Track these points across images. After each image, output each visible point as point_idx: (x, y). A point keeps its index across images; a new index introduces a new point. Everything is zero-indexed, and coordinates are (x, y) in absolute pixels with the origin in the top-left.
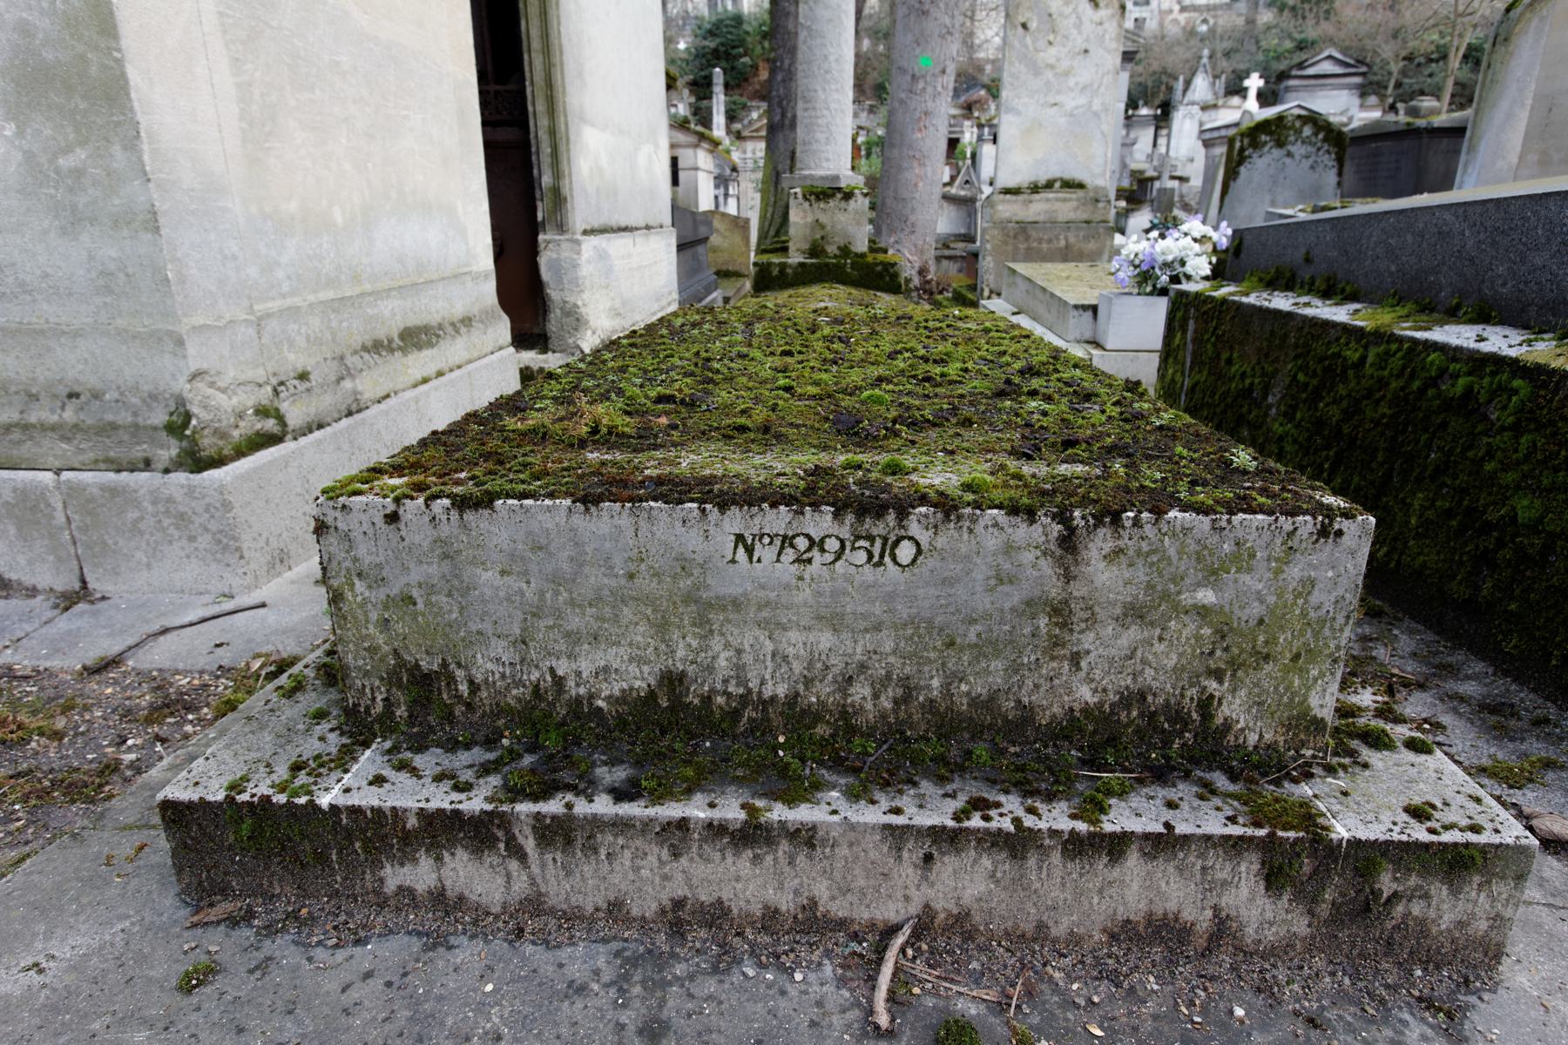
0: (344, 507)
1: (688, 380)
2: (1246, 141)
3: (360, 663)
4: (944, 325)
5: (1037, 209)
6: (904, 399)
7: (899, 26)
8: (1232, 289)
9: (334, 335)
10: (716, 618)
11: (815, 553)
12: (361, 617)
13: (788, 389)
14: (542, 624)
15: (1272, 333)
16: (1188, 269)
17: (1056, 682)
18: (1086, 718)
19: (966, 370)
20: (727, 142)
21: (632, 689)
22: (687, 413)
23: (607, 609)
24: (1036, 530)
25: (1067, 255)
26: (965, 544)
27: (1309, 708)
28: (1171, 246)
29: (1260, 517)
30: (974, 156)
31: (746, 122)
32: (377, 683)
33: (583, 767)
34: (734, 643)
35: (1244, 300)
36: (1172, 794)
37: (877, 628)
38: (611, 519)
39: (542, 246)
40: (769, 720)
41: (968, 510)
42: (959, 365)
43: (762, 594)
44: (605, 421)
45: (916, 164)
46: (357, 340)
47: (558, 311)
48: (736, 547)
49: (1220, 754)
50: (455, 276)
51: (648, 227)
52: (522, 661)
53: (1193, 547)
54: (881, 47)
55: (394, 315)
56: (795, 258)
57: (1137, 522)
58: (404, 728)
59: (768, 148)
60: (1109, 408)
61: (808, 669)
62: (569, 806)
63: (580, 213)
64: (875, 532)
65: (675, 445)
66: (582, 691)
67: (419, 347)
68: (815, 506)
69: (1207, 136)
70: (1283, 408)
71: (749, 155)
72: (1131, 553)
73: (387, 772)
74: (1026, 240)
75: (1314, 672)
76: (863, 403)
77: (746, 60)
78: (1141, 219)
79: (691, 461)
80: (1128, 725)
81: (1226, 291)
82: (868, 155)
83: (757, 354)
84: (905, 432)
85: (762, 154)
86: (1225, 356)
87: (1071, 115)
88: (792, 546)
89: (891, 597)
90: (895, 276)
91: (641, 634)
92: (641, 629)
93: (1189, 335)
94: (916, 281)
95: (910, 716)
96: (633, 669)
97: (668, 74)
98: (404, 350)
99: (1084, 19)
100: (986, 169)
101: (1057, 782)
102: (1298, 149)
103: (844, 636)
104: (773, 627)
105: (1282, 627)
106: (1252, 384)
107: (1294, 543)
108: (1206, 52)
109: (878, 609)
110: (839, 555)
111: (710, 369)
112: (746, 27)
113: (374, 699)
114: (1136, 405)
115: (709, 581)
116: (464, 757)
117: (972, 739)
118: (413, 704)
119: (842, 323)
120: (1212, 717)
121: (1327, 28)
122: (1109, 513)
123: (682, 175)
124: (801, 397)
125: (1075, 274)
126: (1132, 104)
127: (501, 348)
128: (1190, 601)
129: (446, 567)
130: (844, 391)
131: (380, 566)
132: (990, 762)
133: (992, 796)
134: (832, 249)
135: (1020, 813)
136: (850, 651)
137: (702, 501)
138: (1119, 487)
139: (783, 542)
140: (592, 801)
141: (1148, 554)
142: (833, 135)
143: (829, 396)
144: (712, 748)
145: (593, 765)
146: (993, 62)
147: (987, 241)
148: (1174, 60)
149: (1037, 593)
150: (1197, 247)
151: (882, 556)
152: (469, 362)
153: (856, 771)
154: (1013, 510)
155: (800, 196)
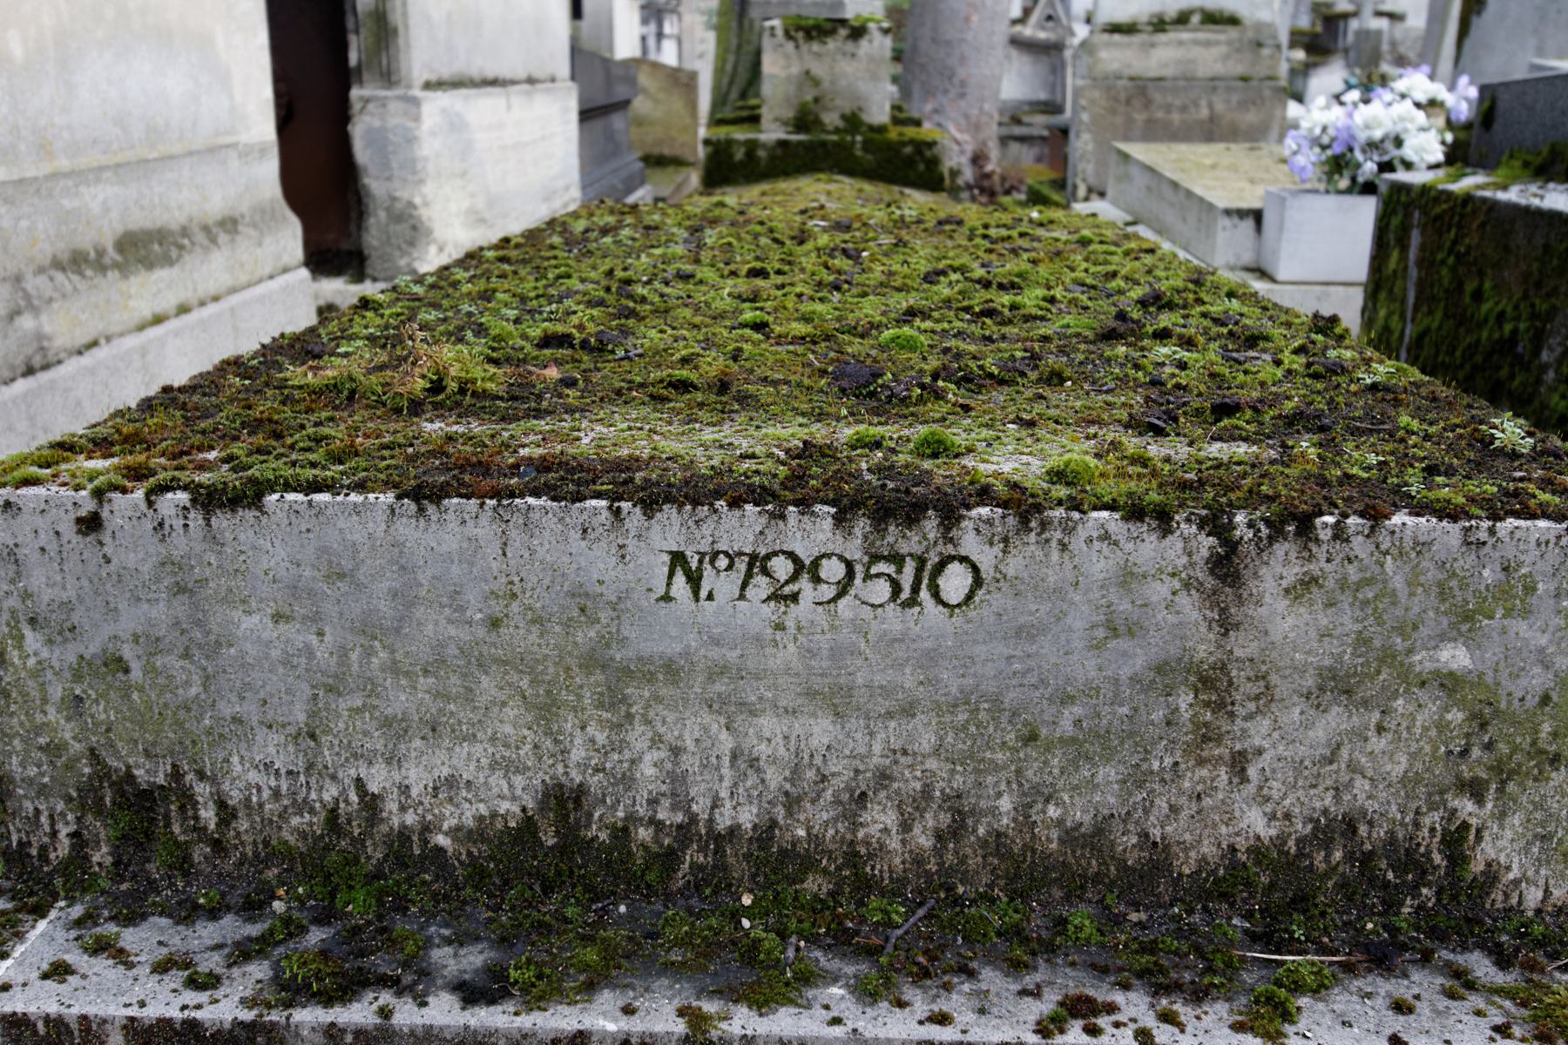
0: (8, 504)
1: (595, 312)
3: (32, 771)
4: (1014, 233)
6: (952, 343)
10: (638, 693)
11: (804, 584)
12: (35, 694)
13: (759, 327)
14: (343, 705)
15: (1547, 248)
16: (1408, 152)
17: (1207, 802)
18: (1258, 863)
19: (1052, 300)
21: (494, 815)
22: (590, 359)
23: (454, 679)
24: (1174, 544)
25: (1211, 131)
26: (1055, 569)
32: (60, 806)
33: (410, 947)
34: (669, 737)
35: (1501, 196)
36: (1401, 989)
37: (908, 711)
38: (462, 526)
39: (356, 106)
40: (725, 868)
41: (1059, 513)
42: (1040, 292)
44: (453, 372)
46: (44, 251)
47: (382, 215)
48: (671, 575)
49: (1481, 923)
50: (212, 150)
51: (531, 81)
52: (310, 767)
53: (1433, 575)
55: (106, 210)
56: (771, 133)
57: (1339, 533)
58: (104, 883)
60: (1287, 357)
61: (792, 781)
62: (385, 1013)
63: (421, 54)
64: (904, 548)
65: (570, 410)
66: (410, 818)
67: (150, 264)
68: (804, 504)
72: (1330, 584)
73: (74, 957)
74: (1144, 106)
76: (883, 348)
78: (1330, 77)
79: (596, 435)
80: (1326, 876)
81: (1470, 182)
83: (705, 272)
84: (953, 393)
86: (1470, 287)
88: (766, 572)
89: (931, 658)
90: (934, 162)
91: (511, 722)
92: (510, 712)
93: (1413, 253)
94: (968, 174)
95: (963, 861)
96: (498, 782)
98: (123, 269)
101: (1210, 970)
103: (852, 724)
104: (733, 710)
106: (1515, 331)
109: (908, 678)
110: (843, 588)
111: (630, 297)
114: (1332, 354)
116: (208, 931)
117: (1067, 898)
118: (122, 841)
119: (848, 228)
120: (1466, 860)
122: (1294, 516)
124: (780, 339)
127: (286, 270)
128: (1429, 666)
129: (181, 607)
130: (852, 330)
131: (67, 606)
132: (1097, 938)
133: (1102, 993)
134: (831, 119)
135: (1149, 1021)
136: (862, 750)
137: (614, 497)
139: (751, 566)
140: (424, 1004)
141: (1359, 586)
143: (828, 338)
144: (631, 917)
145: (428, 943)
147: (1080, 109)
149: (1174, 650)
150: (1420, 116)
151: (916, 589)
152: (233, 290)
153: (871, 952)
154: (1134, 512)
155: (780, 32)
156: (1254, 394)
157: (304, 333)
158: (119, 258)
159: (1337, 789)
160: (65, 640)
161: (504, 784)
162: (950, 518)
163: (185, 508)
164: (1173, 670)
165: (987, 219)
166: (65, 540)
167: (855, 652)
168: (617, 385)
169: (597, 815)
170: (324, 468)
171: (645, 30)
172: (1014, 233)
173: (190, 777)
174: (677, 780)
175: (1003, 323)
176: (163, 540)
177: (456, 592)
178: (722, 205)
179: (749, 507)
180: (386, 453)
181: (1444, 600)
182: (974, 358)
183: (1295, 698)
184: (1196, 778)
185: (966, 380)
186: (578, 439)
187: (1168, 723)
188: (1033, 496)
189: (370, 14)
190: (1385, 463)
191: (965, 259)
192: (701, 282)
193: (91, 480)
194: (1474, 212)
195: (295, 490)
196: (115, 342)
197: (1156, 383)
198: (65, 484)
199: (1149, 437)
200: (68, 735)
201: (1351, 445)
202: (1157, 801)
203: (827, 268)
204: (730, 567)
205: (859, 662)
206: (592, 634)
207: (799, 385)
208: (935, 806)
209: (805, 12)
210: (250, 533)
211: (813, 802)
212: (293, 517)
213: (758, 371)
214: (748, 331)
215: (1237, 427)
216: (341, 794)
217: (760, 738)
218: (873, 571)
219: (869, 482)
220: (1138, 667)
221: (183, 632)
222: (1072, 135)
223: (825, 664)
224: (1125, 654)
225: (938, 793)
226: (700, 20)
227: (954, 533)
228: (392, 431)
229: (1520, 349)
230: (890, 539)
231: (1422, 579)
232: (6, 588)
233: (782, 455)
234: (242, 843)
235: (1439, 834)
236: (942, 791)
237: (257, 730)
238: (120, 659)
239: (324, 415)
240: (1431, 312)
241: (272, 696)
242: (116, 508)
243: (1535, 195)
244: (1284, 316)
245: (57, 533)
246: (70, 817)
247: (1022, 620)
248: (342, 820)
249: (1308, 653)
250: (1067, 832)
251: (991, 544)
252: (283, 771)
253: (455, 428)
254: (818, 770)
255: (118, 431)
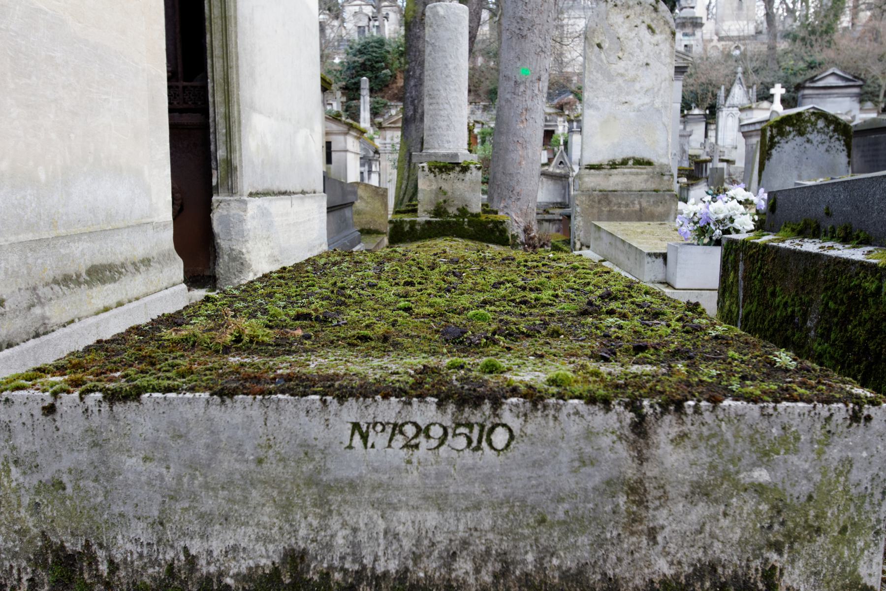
0: (7, 400)
1: (324, 303)
2: (775, 131)
3: (10, 544)
4: (540, 264)
5: (616, 180)
6: (504, 317)
7: (504, 46)
8: (771, 237)
9: (29, 271)
10: (335, 499)
11: (422, 439)
12: (14, 502)
13: (407, 309)
14: (179, 506)
15: (805, 270)
16: (736, 225)
17: (637, 555)
19: (557, 296)
20: (371, 131)
21: (257, 566)
24: (612, 417)
25: (641, 216)
26: (551, 430)
27: (859, 577)
28: (722, 207)
29: (801, 404)
30: (566, 143)
31: (386, 117)
32: (24, 564)
34: (351, 522)
35: (781, 245)
37: (477, 507)
38: (244, 410)
39: (215, 205)
41: (553, 401)
42: (551, 292)
43: (375, 476)
44: (247, 332)
45: (519, 148)
46: (49, 275)
47: (226, 257)
48: (353, 434)
50: (139, 225)
51: (303, 192)
52: (159, 541)
53: (746, 432)
54: (492, 63)
55: (83, 254)
56: (422, 217)
57: (697, 410)
59: (404, 136)
60: (673, 323)
61: (416, 546)
63: (247, 180)
64: (473, 419)
66: (212, 569)
67: (103, 282)
68: (421, 397)
69: (746, 129)
70: (819, 331)
71: (388, 141)
72: (694, 437)
75: (861, 544)
76: (469, 320)
77: (387, 71)
78: (699, 191)
79: (316, 364)
82: (483, 142)
83: (383, 284)
84: (503, 341)
85: (399, 140)
86: (769, 290)
87: (639, 110)
88: (402, 433)
89: (488, 478)
90: (504, 231)
91: (267, 515)
92: (267, 510)
94: (522, 237)
96: (260, 548)
97: (323, 80)
99: (644, 41)
100: (575, 153)
102: (815, 137)
103: (449, 514)
104: (385, 507)
105: (828, 503)
106: (793, 312)
107: (831, 427)
108: (740, 69)
109: (477, 489)
110: (442, 441)
111: (343, 295)
112: (387, 48)
113: (20, 579)
115: (328, 465)
119: (457, 262)
121: (830, 54)
122: (673, 402)
123: (334, 156)
125: (648, 230)
126: (686, 105)
127: (174, 285)
128: (748, 480)
129: (95, 454)
130: (454, 311)
131: (35, 454)
134: (452, 210)
136: (453, 528)
138: (680, 382)
139: (394, 430)
142: (453, 120)
143: (441, 315)
146: (579, 74)
148: (719, 74)
149: (615, 473)
151: (480, 441)
152: (147, 295)
154: (591, 400)
155: (426, 169)
156: (656, 341)
157: (174, 314)
158: (88, 279)
159: (705, 548)
160: (33, 472)
161: (263, 549)
162: (497, 404)
163: (100, 401)
164: (615, 484)
165: (526, 258)
166: (35, 418)
167: (449, 475)
168: (332, 338)
169: (312, 566)
170: (174, 380)
171: (362, 169)
172: (540, 264)
173: (95, 547)
174: (355, 546)
175: (531, 307)
176: (87, 418)
177: (240, 445)
178: (396, 252)
179: (393, 399)
180: (208, 372)
181: (753, 445)
182: (515, 324)
183: (680, 498)
184: (630, 542)
185: (509, 335)
186: (308, 365)
187: (614, 512)
188: (539, 392)
189: (223, 160)
190: (720, 374)
191: (514, 277)
192: (380, 288)
193: (52, 387)
194: (769, 253)
195: (158, 391)
196: (83, 321)
197: (606, 336)
198: (38, 389)
199: (601, 363)
200: (30, 524)
201: (704, 366)
202: (610, 555)
203: (444, 281)
204: (383, 430)
205: (451, 481)
206: (311, 467)
207: (425, 338)
208: (492, 559)
209: (439, 160)
210: (133, 414)
211: (428, 557)
212: (156, 406)
213: (405, 332)
214: (401, 312)
215: (646, 357)
216: (176, 555)
217: (399, 522)
218: (458, 432)
219: (455, 386)
220: (597, 482)
221: (95, 467)
222: (572, 218)
223: (433, 482)
224: (589, 475)
225: (494, 552)
226: (389, 164)
227: (499, 412)
228: (214, 361)
229: (796, 320)
230: (466, 415)
231: (741, 434)
232: (3, 444)
233: (412, 372)
234: (121, 584)
235: (760, 572)
236: (496, 551)
237: (132, 521)
238: (61, 483)
239: (179, 354)
240: (751, 303)
241: (141, 502)
242: (63, 401)
243: (798, 245)
244: (673, 304)
245: (32, 415)
246: (29, 570)
247: (535, 457)
248: (176, 570)
249: (685, 474)
250: (563, 573)
251: (518, 417)
252: (145, 543)
253: (246, 360)
254: (430, 540)
255: (70, 362)
